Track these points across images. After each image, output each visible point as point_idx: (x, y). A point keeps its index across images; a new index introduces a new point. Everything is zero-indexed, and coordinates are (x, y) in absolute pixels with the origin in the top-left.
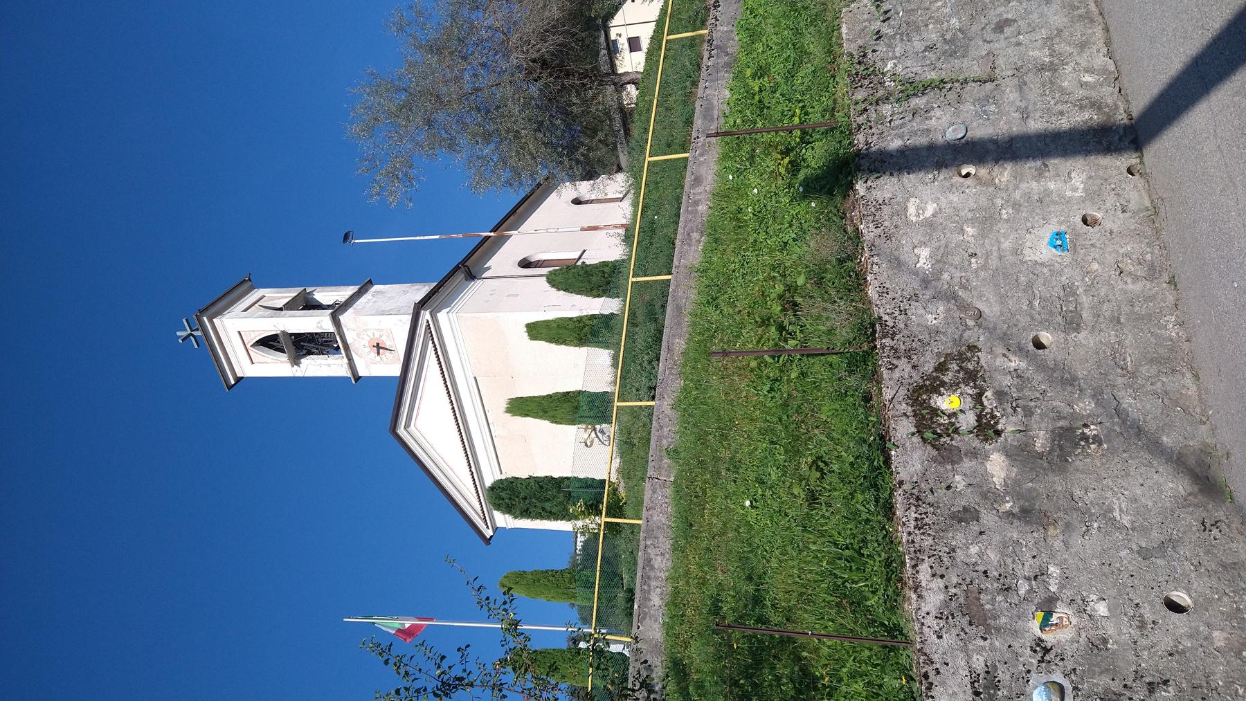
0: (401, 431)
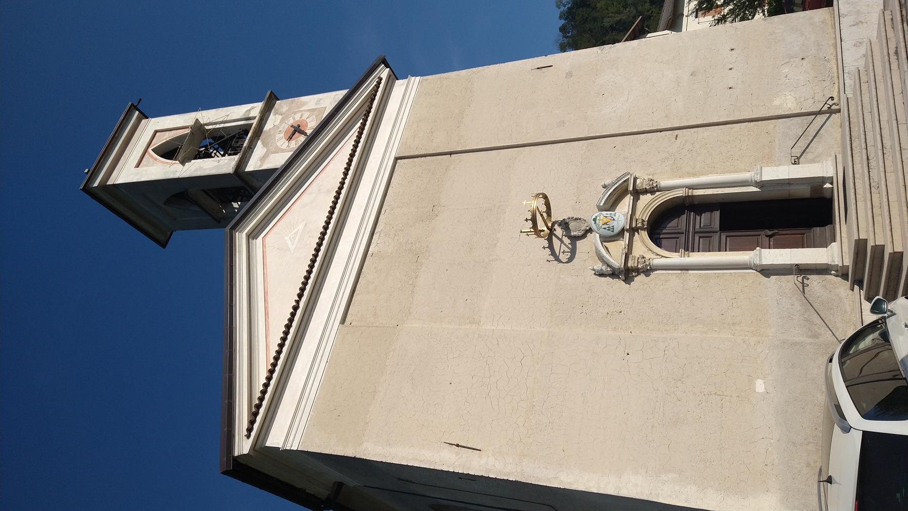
0: (241, 238)
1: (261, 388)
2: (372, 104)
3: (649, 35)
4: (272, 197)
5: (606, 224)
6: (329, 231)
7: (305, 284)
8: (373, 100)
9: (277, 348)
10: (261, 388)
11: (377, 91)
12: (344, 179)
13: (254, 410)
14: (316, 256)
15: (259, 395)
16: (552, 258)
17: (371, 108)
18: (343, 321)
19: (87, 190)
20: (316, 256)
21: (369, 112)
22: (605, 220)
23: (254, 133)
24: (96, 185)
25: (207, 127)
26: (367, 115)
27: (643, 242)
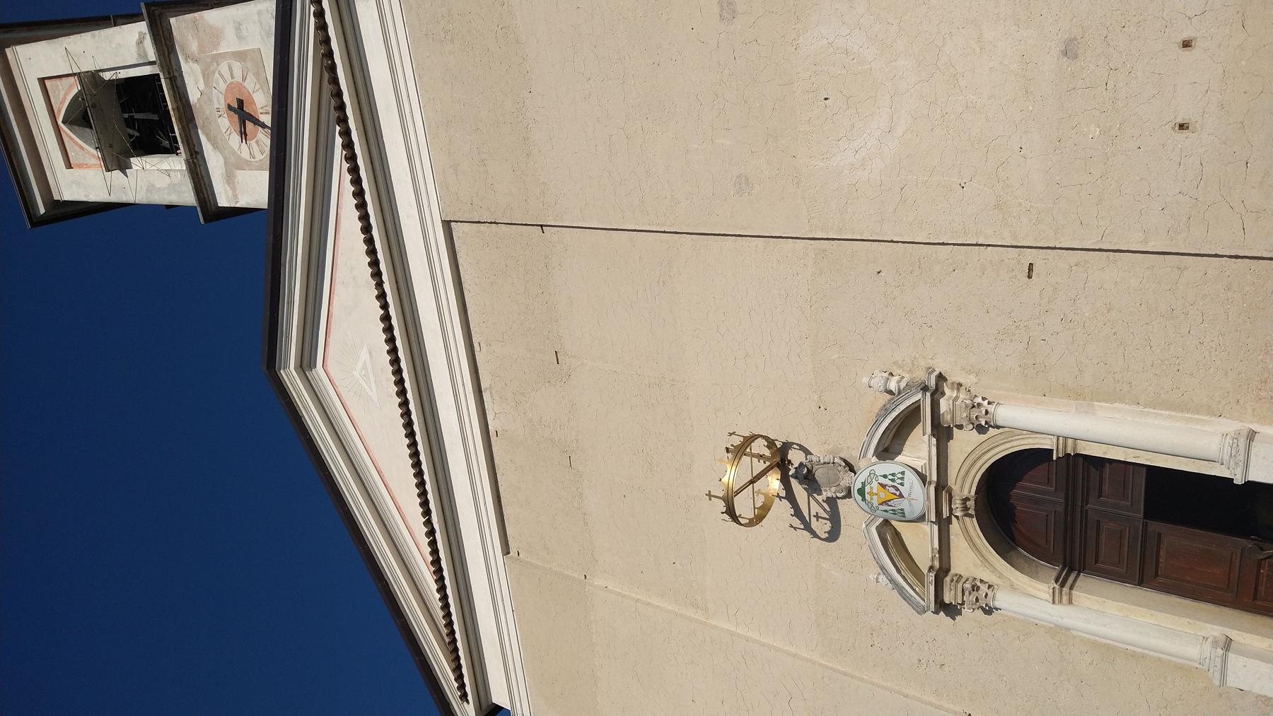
1: (438, 596)
2: (335, 81)
3: (934, 441)
4: (291, 302)
5: (885, 503)
6: (399, 343)
7: (398, 372)
8: (333, 68)
9: (407, 441)
10: (438, 596)
11: (330, 54)
12: (380, 285)
13: (447, 640)
14: (413, 445)
15: (441, 613)
16: (797, 523)
17: (338, 94)
18: (506, 551)
19: (38, 222)
20: (413, 445)
21: (341, 107)
22: (884, 495)
23: (180, 120)
24: (42, 211)
25: (107, 76)
26: (343, 120)
27: (965, 531)
